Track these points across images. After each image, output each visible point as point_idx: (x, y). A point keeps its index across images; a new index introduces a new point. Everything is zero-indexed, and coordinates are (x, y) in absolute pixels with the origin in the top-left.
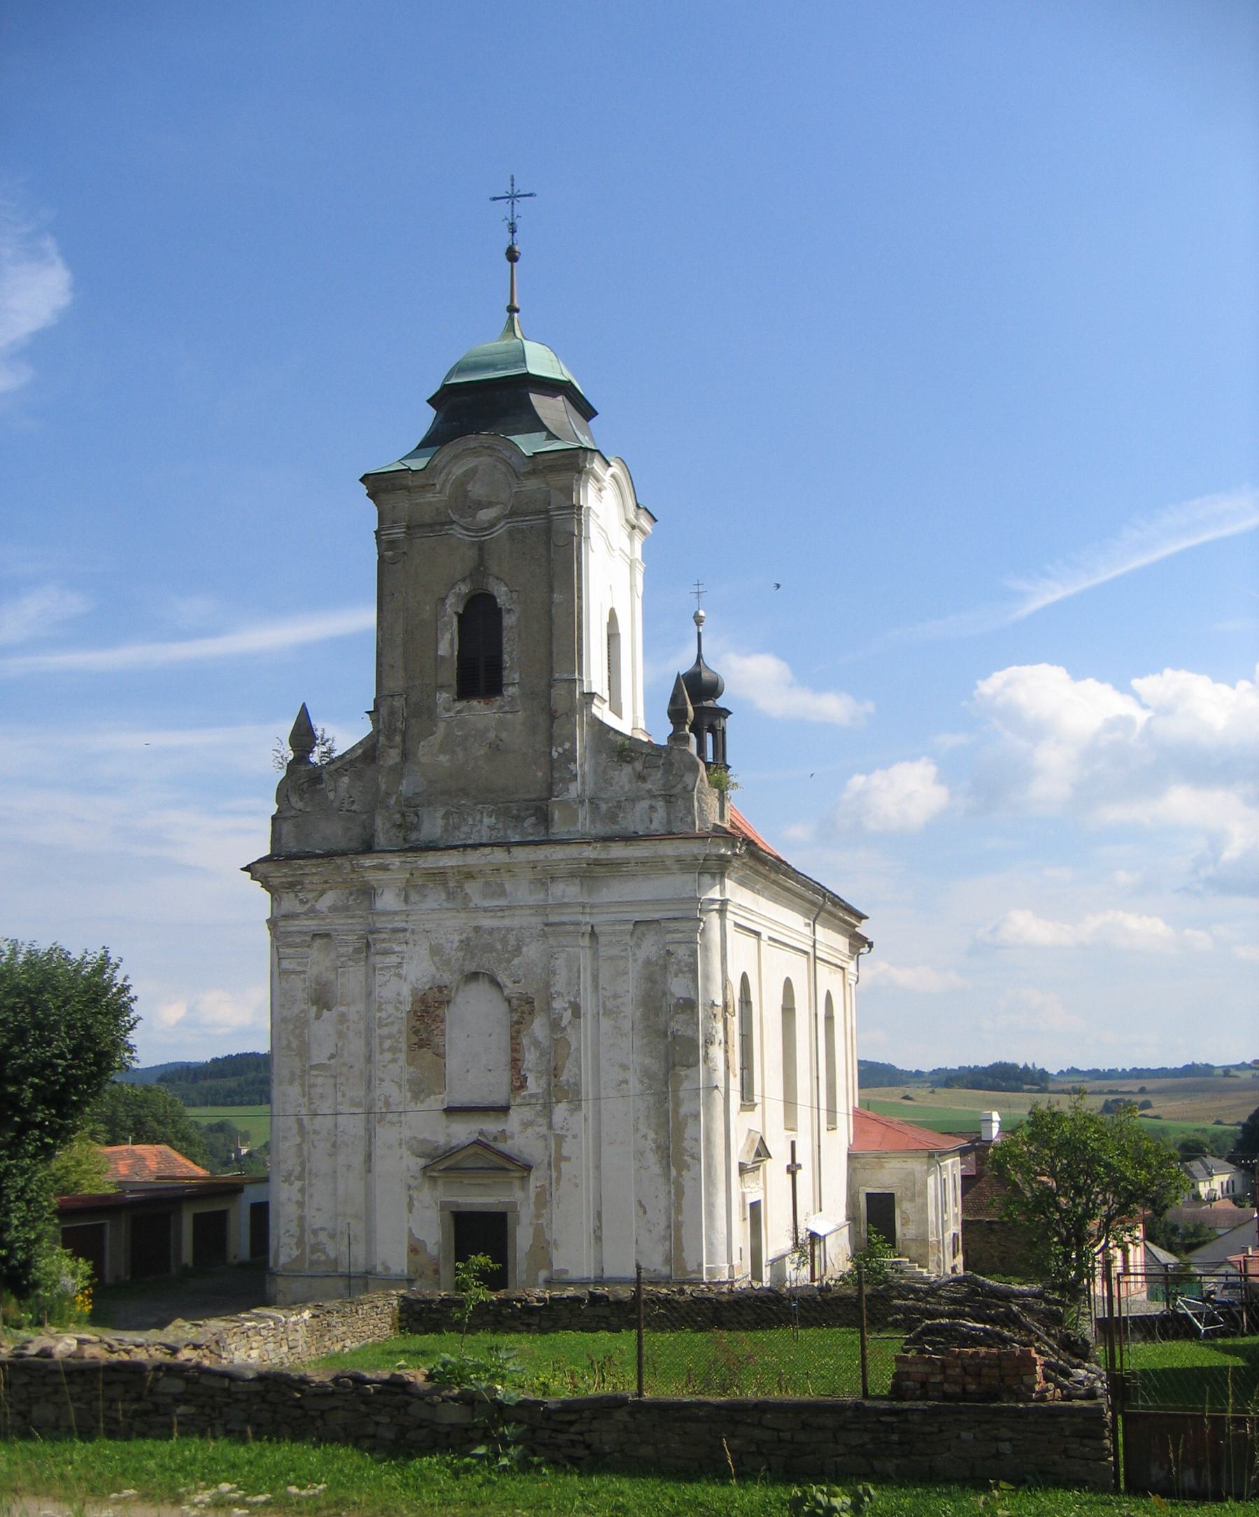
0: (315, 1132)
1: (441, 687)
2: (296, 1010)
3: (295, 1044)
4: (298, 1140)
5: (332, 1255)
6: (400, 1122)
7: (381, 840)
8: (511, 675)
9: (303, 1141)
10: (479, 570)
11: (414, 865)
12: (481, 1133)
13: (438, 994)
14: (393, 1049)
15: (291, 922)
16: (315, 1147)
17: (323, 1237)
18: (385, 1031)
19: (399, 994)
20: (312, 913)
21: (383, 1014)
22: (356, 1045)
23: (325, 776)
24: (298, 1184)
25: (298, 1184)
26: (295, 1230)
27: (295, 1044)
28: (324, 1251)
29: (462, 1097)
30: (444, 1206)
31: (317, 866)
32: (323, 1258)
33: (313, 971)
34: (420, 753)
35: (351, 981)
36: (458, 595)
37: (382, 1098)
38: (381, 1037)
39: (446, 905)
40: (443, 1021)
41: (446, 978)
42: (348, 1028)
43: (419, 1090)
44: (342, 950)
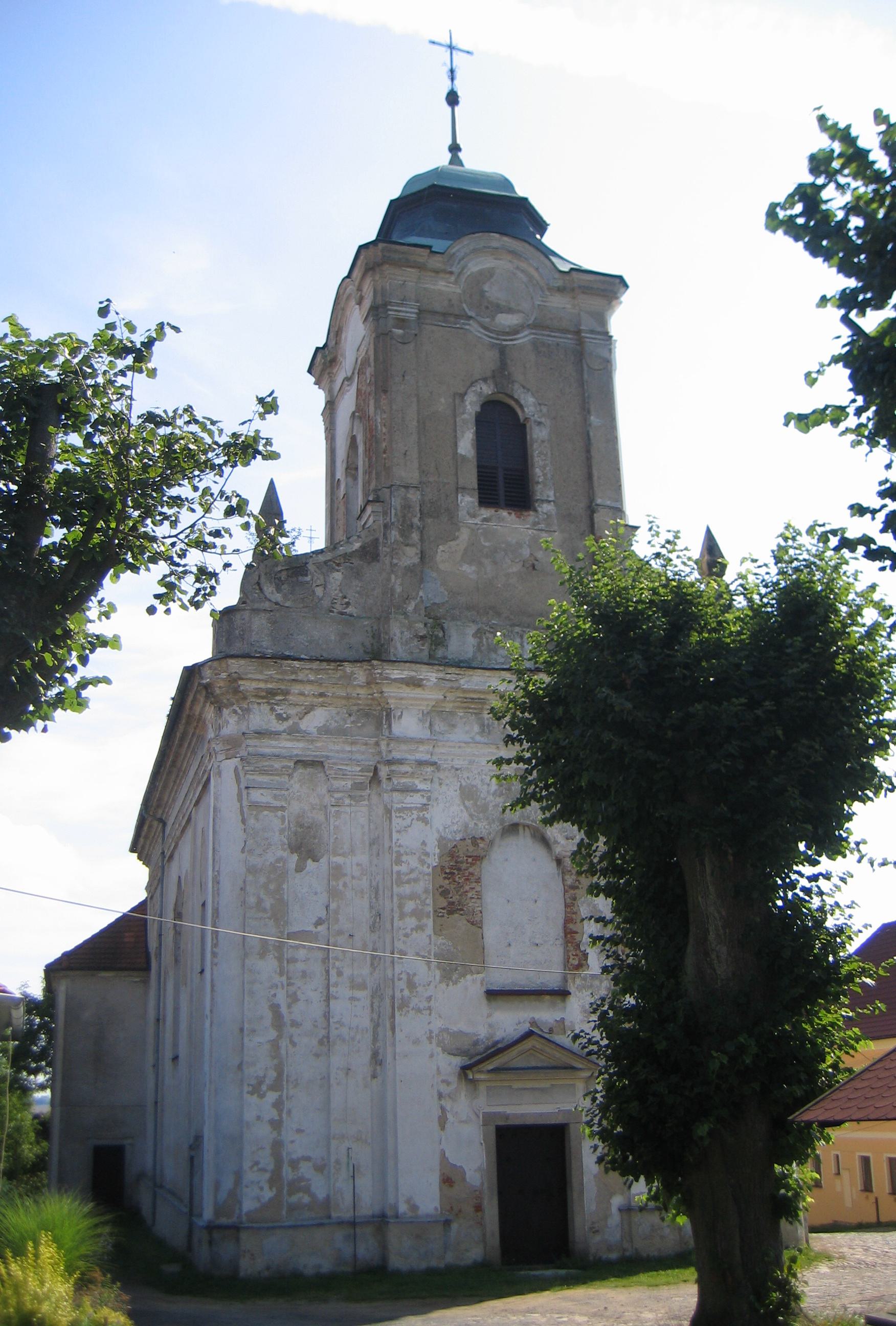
0: (294, 1024)
1: (459, 489)
2: (270, 858)
3: (268, 903)
4: (273, 1034)
5: (321, 1194)
6: (429, 1008)
7: (399, 649)
8: (545, 490)
9: (280, 1036)
10: (501, 373)
11: (455, 685)
12: (533, 1023)
13: (471, 848)
14: (416, 913)
15: (266, 741)
16: (294, 1044)
17: (305, 1169)
18: (407, 889)
19: (424, 843)
20: (294, 731)
21: (404, 868)
22: (356, 909)
23: (311, 567)
24: (272, 1096)
25: (272, 1096)
26: (267, 1161)
27: (268, 903)
28: (307, 1190)
29: (501, 979)
30: (488, 1118)
31: (317, 671)
32: (306, 1199)
33: (295, 807)
34: (438, 558)
35: (351, 824)
36: (480, 394)
37: (404, 976)
38: (401, 897)
39: (478, 738)
40: (478, 881)
41: (483, 828)
42: (345, 885)
43: (451, 970)
44: (337, 784)
